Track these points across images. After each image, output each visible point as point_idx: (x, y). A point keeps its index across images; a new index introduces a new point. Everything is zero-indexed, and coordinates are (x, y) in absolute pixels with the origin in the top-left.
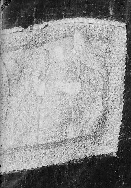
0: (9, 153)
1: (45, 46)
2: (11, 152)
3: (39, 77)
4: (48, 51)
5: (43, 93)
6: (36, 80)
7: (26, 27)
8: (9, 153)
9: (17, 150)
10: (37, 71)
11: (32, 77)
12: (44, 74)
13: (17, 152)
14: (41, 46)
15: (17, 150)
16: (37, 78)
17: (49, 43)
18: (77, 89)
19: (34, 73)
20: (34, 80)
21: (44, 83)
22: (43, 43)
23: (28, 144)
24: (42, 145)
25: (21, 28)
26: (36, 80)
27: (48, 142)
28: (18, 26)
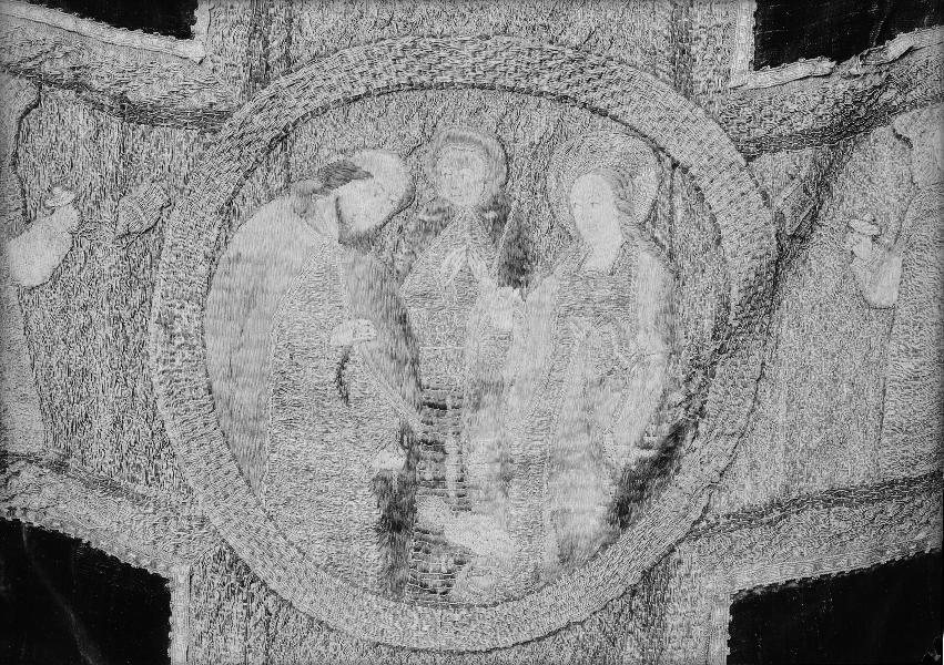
0: (772, 517)
1: (899, 122)
2: (778, 514)
3: (875, 239)
4: (907, 141)
5: (895, 297)
6: (864, 249)
7: (840, 56)
8: (772, 517)
9: (799, 504)
10: (868, 217)
11: (851, 238)
12: (893, 226)
13: (797, 513)
14: (886, 123)
15: (799, 504)
16: (869, 239)
17: (915, 111)
18: (447, 442)
19: (854, 223)
20: (855, 249)
21: (897, 261)
22: (894, 111)
23: (842, 480)
24: (892, 484)
25: (826, 65)
26: (864, 249)
27: (915, 474)
28: (810, 54)
